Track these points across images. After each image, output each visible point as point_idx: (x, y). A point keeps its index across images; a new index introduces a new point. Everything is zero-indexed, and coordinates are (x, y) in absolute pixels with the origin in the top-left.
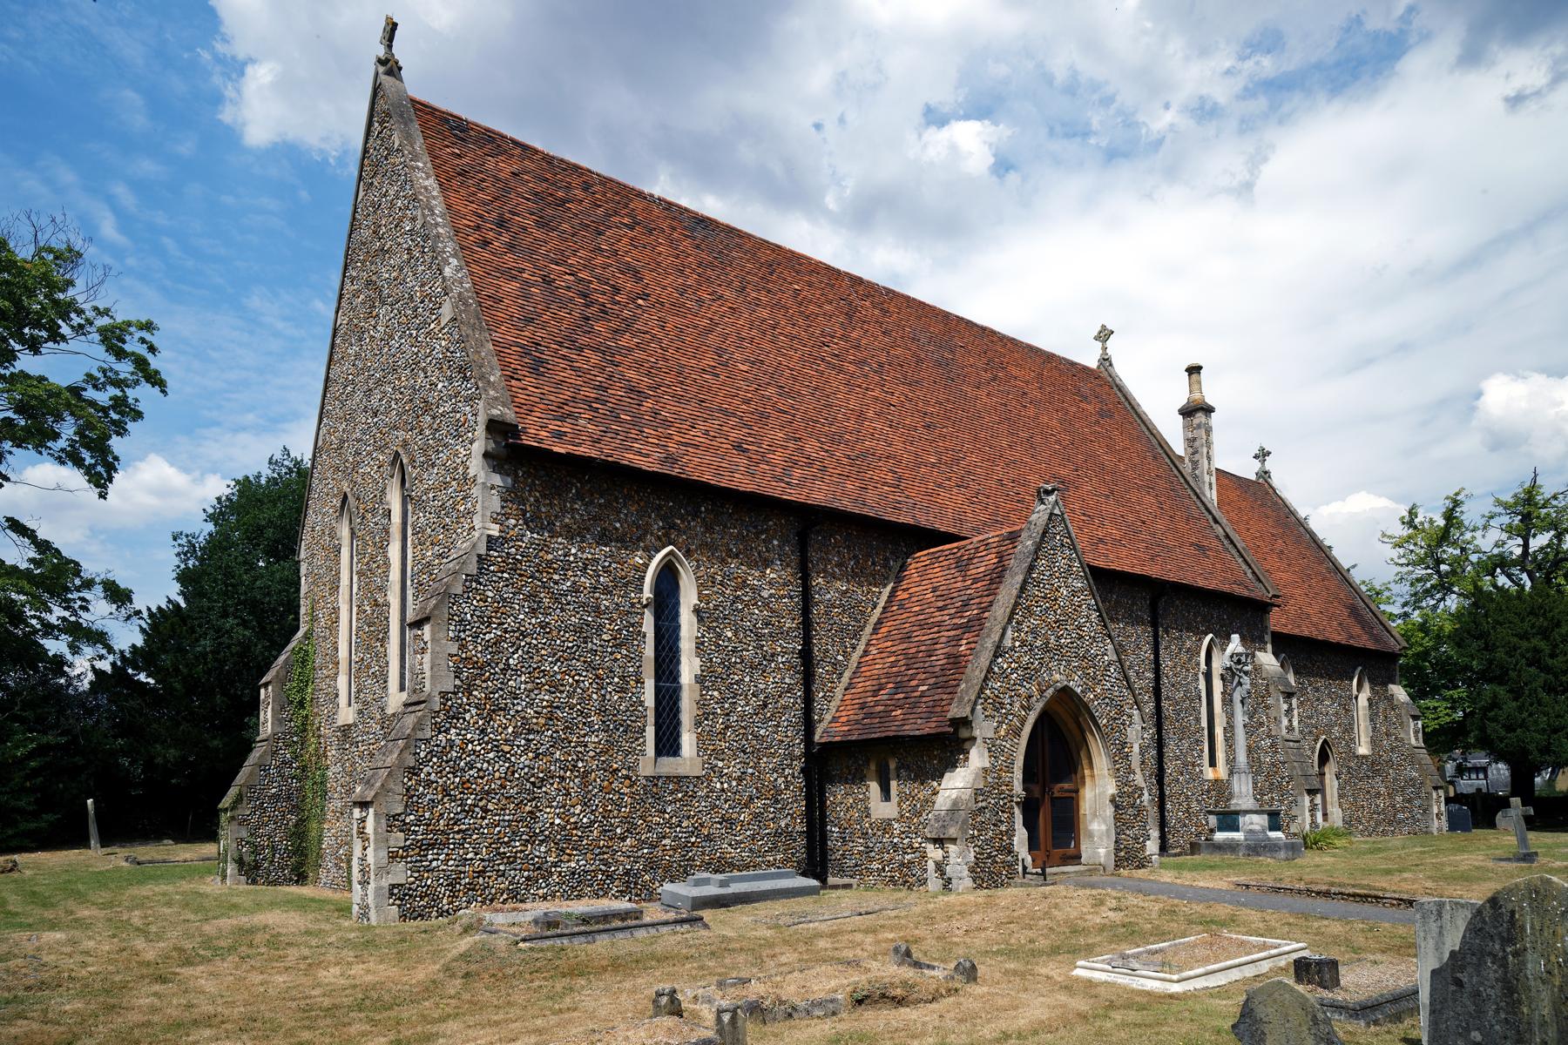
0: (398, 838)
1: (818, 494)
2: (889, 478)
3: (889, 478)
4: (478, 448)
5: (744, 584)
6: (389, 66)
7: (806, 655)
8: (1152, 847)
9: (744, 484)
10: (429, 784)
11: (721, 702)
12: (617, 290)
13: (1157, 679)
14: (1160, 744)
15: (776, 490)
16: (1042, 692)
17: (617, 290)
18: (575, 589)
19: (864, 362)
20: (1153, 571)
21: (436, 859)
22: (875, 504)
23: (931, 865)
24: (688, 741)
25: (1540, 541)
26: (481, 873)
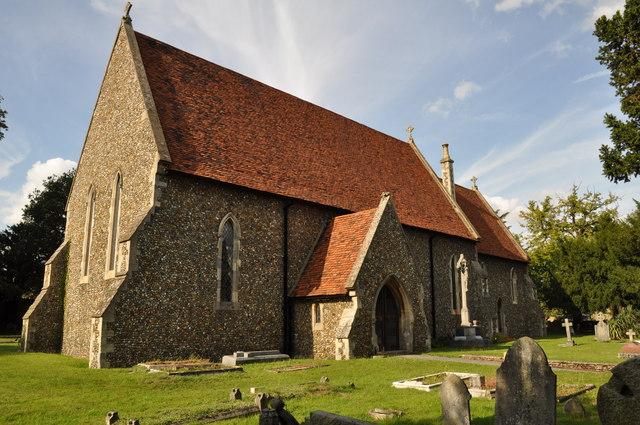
0: (111, 333)
1: (292, 192)
2: (322, 187)
3: (322, 187)
4: (154, 170)
5: (260, 229)
6: (128, 20)
7: (285, 259)
8: (428, 342)
9: (262, 187)
10: (125, 310)
11: (249, 279)
12: (212, 107)
13: (432, 272)
14: (433, 298)
15: (276, 191)
16: (384, 278)
17: (212, 107)
18: (190, 230)
19: (312, 137)
20: (430, 227)
21: (127, 342)
22: (315, 197)
23: (337, 350)
24: (235, 296)
25: (579, 216)
26: (145, 350)
